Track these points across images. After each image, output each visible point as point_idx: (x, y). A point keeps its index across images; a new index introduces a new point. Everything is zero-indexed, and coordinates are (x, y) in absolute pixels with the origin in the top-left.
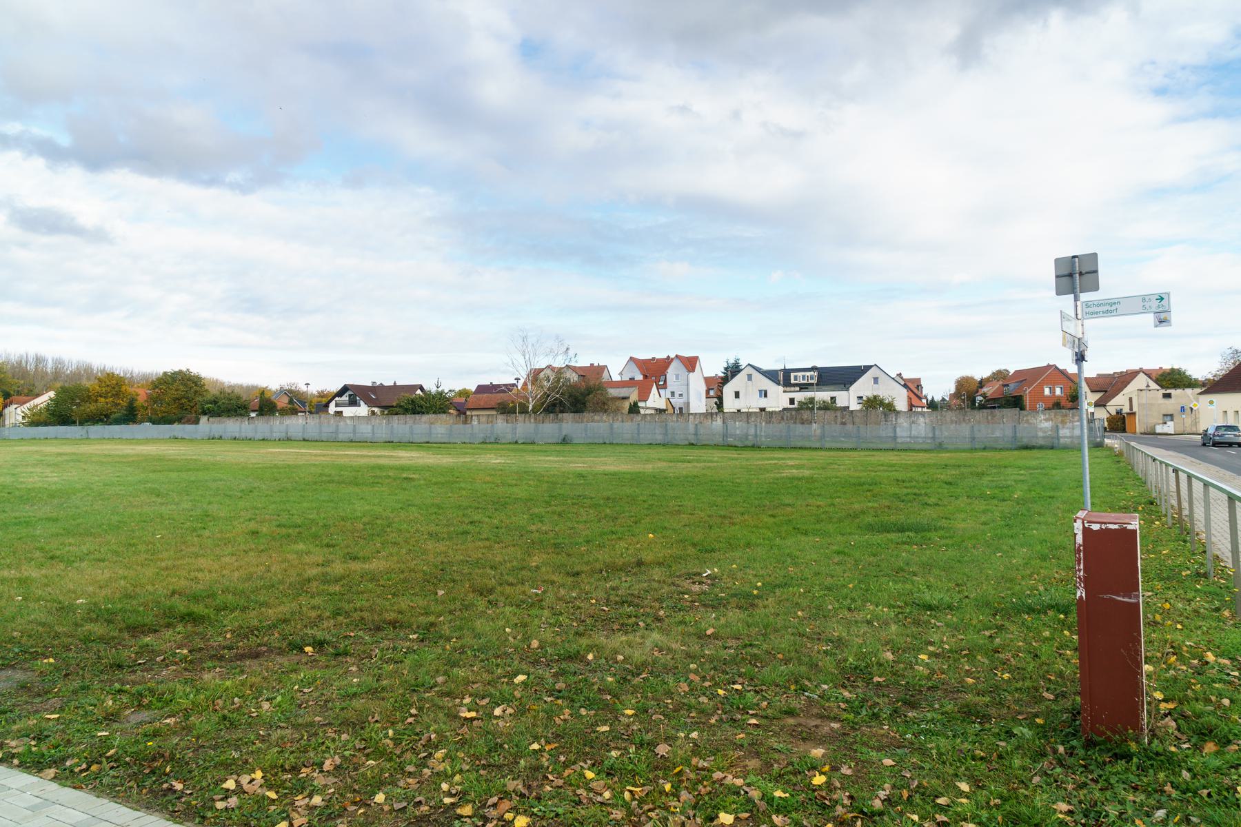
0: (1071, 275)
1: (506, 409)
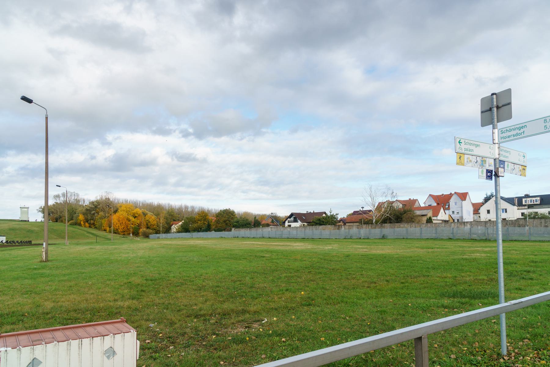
0: (490, 109)
1: (369, 222)
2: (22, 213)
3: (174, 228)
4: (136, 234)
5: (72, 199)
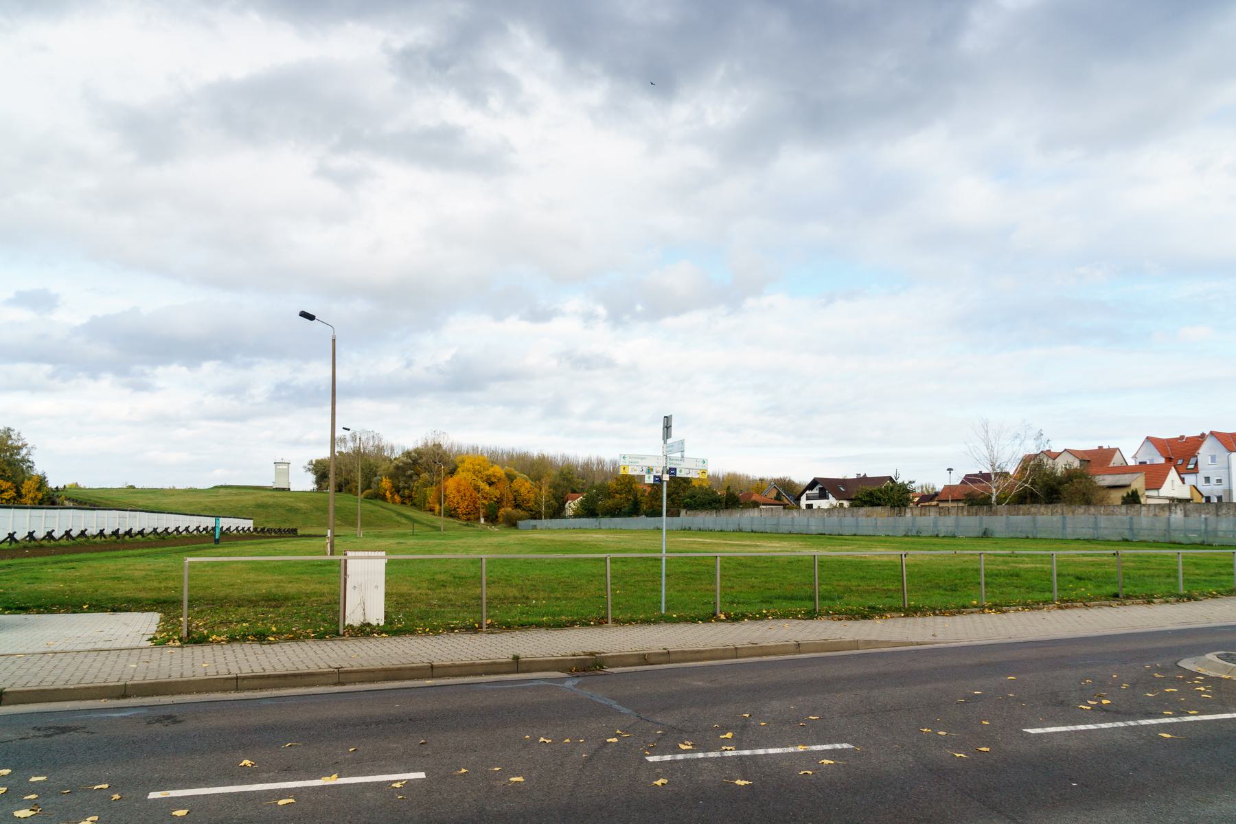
2: (278, 473)
3: (572, 506)
4: (492, 518)
5: (370, 446)
